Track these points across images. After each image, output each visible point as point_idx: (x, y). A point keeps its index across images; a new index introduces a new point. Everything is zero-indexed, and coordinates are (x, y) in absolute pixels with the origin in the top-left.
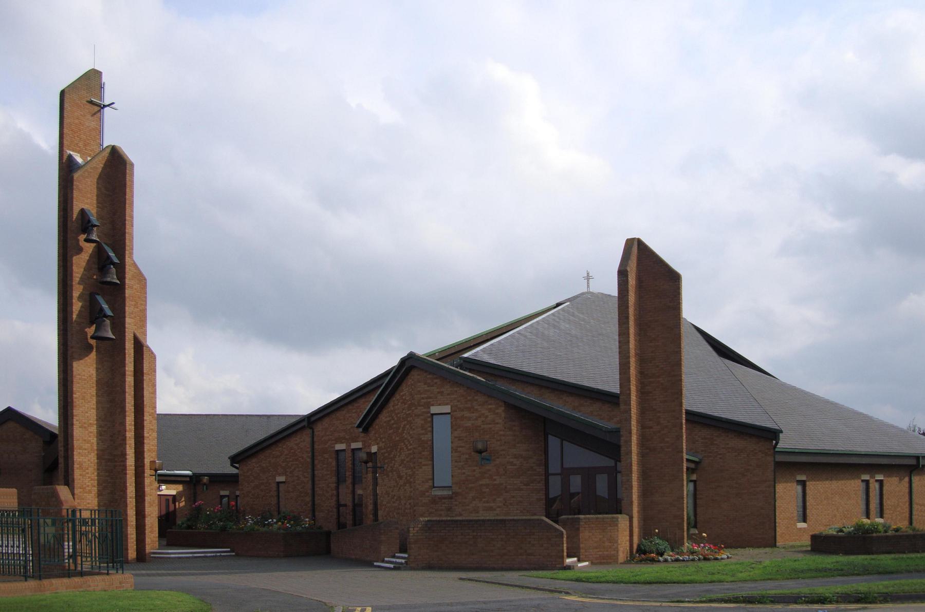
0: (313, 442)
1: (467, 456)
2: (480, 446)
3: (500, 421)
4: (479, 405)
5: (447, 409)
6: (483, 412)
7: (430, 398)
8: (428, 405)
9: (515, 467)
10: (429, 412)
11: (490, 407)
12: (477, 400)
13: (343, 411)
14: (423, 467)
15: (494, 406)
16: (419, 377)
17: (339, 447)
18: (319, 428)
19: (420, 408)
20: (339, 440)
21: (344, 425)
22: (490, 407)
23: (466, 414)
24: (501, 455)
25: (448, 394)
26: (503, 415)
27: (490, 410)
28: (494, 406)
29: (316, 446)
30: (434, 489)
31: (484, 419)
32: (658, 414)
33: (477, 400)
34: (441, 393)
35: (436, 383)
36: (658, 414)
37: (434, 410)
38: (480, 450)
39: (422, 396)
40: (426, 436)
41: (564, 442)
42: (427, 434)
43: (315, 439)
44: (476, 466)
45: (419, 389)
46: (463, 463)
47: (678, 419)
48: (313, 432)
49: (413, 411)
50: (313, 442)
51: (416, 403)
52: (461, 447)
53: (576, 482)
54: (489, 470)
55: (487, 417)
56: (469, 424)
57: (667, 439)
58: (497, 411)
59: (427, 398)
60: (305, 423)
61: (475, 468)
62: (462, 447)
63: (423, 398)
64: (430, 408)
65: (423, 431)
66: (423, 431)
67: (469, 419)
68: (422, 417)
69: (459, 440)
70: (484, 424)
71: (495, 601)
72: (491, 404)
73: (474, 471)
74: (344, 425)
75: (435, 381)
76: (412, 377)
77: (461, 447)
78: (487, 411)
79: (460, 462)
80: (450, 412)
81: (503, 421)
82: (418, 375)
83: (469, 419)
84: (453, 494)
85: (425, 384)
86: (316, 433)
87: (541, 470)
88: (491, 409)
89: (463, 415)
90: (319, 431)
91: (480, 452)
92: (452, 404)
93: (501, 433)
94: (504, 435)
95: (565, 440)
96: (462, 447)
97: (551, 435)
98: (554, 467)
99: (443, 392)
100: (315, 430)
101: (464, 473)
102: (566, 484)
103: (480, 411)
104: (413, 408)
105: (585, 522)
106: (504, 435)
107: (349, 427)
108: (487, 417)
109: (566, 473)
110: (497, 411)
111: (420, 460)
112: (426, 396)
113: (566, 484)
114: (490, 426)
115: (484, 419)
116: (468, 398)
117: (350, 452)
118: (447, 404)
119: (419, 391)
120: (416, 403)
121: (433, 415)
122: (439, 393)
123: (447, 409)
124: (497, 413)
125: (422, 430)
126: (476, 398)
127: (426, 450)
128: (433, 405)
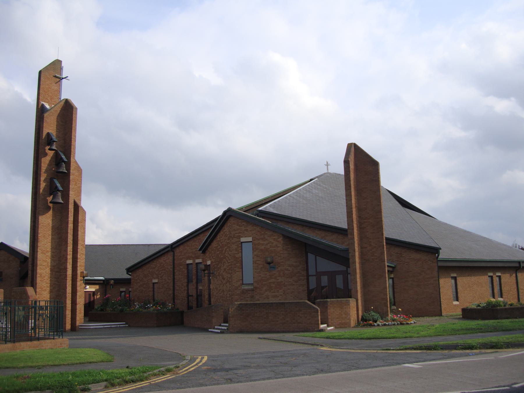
0: (174, 260)
2: (269, 260)
5: (250, 239)
6: (270, 240)
8: (239, 237)
9: (290, 272)
10: (240, 241)
11: (274, 237)
12: (266, 234)
18: (177, 251)
22: (274, 237)
25: (251, 231)
26: (282, 242)
28: (277, 237)
29: (175, 262)
30: (243, 285)
32: (370, 240)
33: (266, 234)
34: (247, 230)
35: (244, 225)
37: (243, 240)
39: (236, 232)
40: (238, 255)
41: (317, 256)
42: (239, 254)
43: (175, 257)
50: (174, 260)
52: (258, 261)
53: (325, 280)
54: (275, 274)
56: (263, 247)
57: (375, 254)
58: (278, 240)
60: (169, 249)
62: (259, 261)
63: (236, 233)
67: (263, 244)
69: (257, 257)
70: (271, 247)
72: (275, 236)
73: (266, 274)
75: (243, 223)
76: (230, 222)
80: (252, 241)
82: (234, 220)
83: (263, 244)
84: (254, 288)
86: (176, 254)
87: (304, 273)
88: (275, 239)
91: (269, 263)
98: (312, 271)
100: (175, 252)
101: (260, 276)
102: (319, 281)
104: (231, 239)
109: (319, 275)
110: (278, 240)
111: (235, 269)
113: (319, 281)
114: (275, 248)
116: (262, 233)
118: (250, 236)
120: (233, 236)
121: (242, 242)
122: (245, 230)
123: (250, 239)
124: (278, 241)
126: (266, 232)
128: (242, 237)
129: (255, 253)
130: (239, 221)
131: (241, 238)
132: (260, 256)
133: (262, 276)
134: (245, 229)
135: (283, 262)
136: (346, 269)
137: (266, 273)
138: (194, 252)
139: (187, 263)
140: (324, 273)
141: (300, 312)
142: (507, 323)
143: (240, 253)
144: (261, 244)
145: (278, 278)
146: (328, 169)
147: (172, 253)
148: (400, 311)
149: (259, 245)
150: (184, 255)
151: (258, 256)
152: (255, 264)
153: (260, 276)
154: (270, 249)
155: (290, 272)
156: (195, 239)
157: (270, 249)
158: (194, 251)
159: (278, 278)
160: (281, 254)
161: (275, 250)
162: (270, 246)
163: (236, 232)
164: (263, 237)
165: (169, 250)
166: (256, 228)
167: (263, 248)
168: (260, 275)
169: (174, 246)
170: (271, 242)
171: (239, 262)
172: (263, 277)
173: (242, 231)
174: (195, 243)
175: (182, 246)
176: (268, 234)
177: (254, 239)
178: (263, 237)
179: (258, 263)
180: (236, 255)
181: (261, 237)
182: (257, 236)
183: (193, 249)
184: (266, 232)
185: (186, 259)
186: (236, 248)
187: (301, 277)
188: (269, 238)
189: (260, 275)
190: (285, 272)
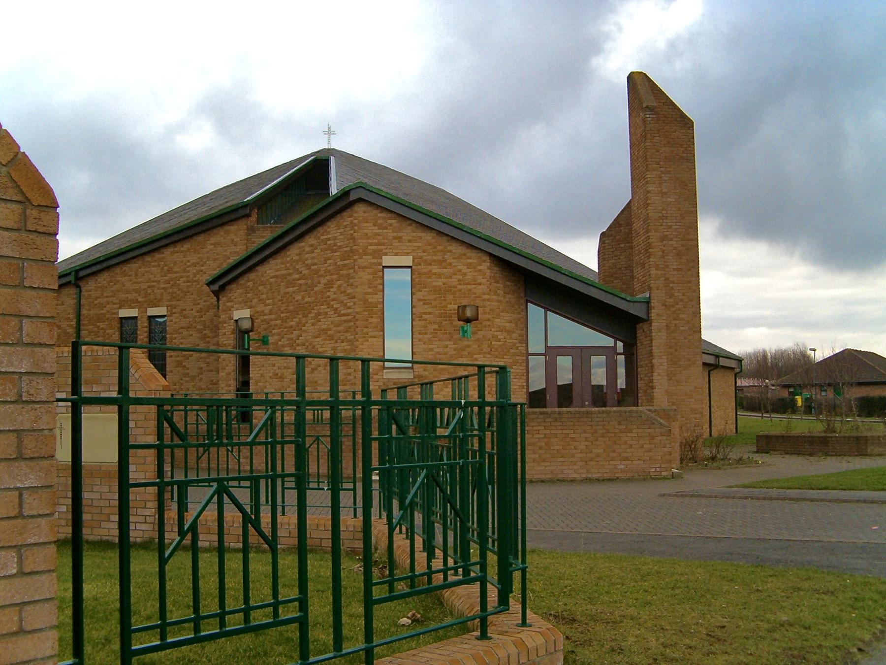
0: (79, 306)
1: (436, 327)
2: (469, 313)
3: (484, 281)
4: (454, 259)
5: (408, 261)
6: (459, 267)
7: (384, 244)
8: (379, 254)
9: (500, 343)
10: (380, 264)
11: (470, 261)
12: (450, 251)
13: (135, 263)
14: (370, 339)
15: (475, 261)
16: (366, 215)
17: (124, 313)
18: (90, 287)
19: (367, 257)
20: (123, 304)
21: (136, 283)
22: (470, 261)
23: (435, 269)
24: (485, 326)
25: (409, 241)
26: (488, 273)
27: (469, 266)
28: (475, 261)
29: (84, 312)
30: (385, 371)
31: (461, 277)
32: (671, 285)
33: (450, 251)
34: (399, 239)
35: (391, 225)
36: (671, 285)
37: (387, 260)
38: (246, 329)
39: (370, 241)
40: (375, 296)
41: (549, 312)
42: (376, 294)
43: (83, 301)
44: (449, 340)
45: (365, 231)
46: (431, 336)
47: (694, 291)
48: (80, 291)
49: (355, 261)
50: (79, 306)
51: (361, 251)
52: (425, 313)
53: (565, 367)
54: (469, 346)
55: (465, 274)
56: (439, 283)
57: (681, 316)
58: (479, 268)
59: (377, 245)
60: (72, 278)
61: (448, 343)
62: (429, 313)
63: (371, 244)
64: (382, 258)
65: (371, 290)
66: (371, 290)
67: (440, 276)
68: (369, 270)
69: (424, 304)
70: (460, 284)
71: (821, 501)
72: (470, 258)
73: (447, 346)
74: (136, 283)
75: (389, 222)
76: (355, 215)
77: (425, 313)
78: (466, 267)
79: (426, 334)
80: (411, 265)
81: (488, 281)
82: (365, 212)
83: (440, 276)
84: (414, 377)
85: (374, 225)
86: (84, 293)
88: (470, 264)
89: (431, 271)
90: (90, 291)
92: (415, 254)
93: (486, 297)
94: (488, 300)
95: (550, 311)
96: (429, 313)
97: (532, 303)
99: (400, 238)
100: (84, 289)
101: (431, 350)
102: (551, 369)
103: (455, 266)
104: (356, 257)
105: (545, 426)
106: (488, 300)
107: (144, 286)
108: (465, 274)
109: (552, 353)
110: (479, 268)
111: (365, 330)
112: (376, 241)
113: (551, 369)
114: (470, 287)
115: (461, 277)
116: (439, 248)
117: (145, 320)
118: (407, 254)
119: (366, 234)
120: (361, 251)
122: (395, 238)
123: (408, 261)
124: (480, 270)
125: (369, 287)
126: (449, 248)
127: (374, 316)
128: (386, 254)
129: (419, 295)
130: (379, 215)
131: (383, 257)
132: (431, 304)
133: (438, 350)
134: (395, 234)
135: (489, 320)
136: (613, 345)
137: (446, 343)
138: (144, 289)
139: (120, 316)
140: (563, 351)
141: (629, 434)
142: (723, 465)
143: (379, 293)
144: (435, 274)
145: (475, 356)
146: (329, 143)
147: (72, 291)
148: (217, 442)
149: (430, 278)
150: (112, 296)
151: (428, 304)
152: (419, 320)
153: (431, 350)
154: (459, 287)
155: (500, 343)
156: (148, 258)
157: (459, 287)
158: (143, 287)
159: (475, 356)
160: (485, 300)
161: (470, 290)
162: (459, 280)
163: (370, 241)
164: (441, 258)
165: (70, 282)
166: (423, 234)
167: (441, 284)
168: (430, 346)
169: (82, 274)
170: (460, 271)
171: (375, 314)
172: (439, 353)
173: (386, 241)
174: (148, 269)
175: (105, 275)
176: (454, 251)
177: (416, 261)
178: (441, 258)
179: (426, 320)
180: (368, 297)
181: (435, 258)
182: (425, 254)
183: (142, 282)
184: (449, 248)
185: (118, 306)
186: (369, 280)
187: (517, 358)
188: (455, 260)
189: (430, 346)
190: (493, 343)
